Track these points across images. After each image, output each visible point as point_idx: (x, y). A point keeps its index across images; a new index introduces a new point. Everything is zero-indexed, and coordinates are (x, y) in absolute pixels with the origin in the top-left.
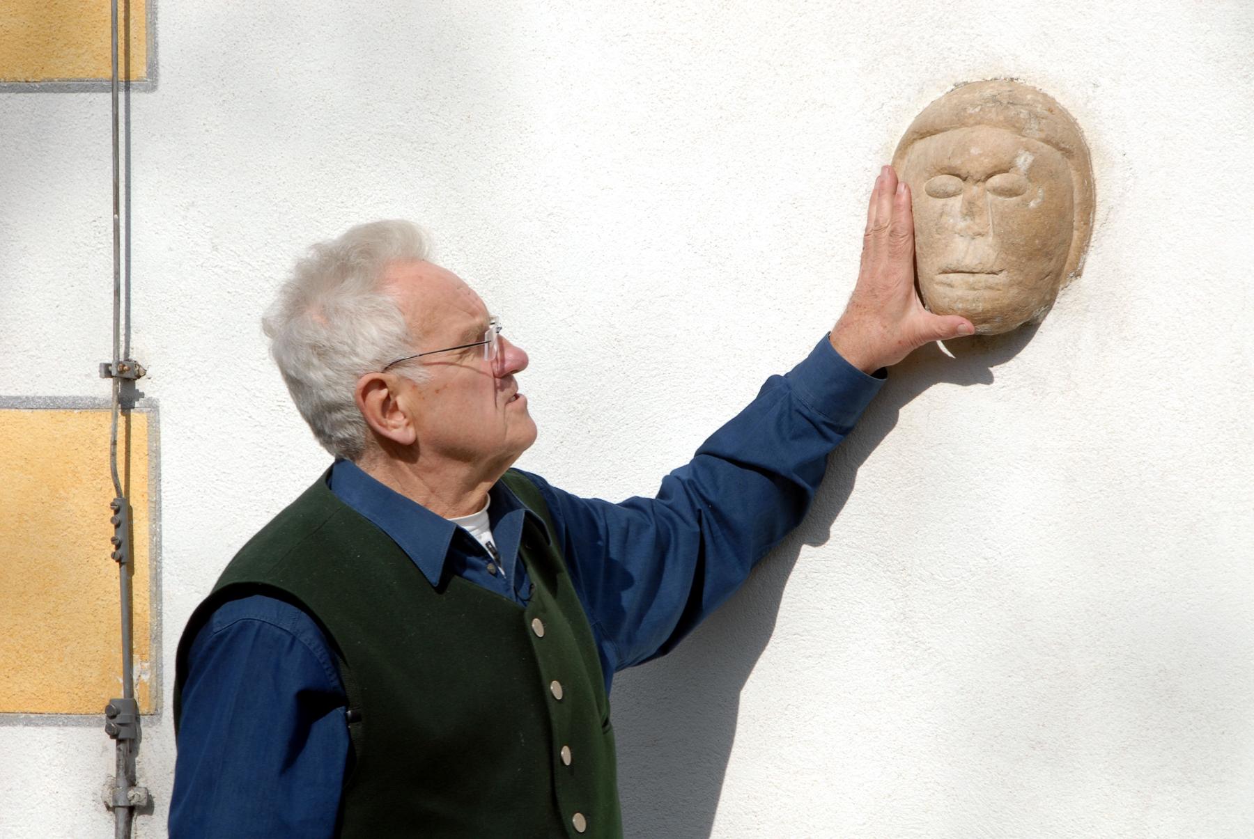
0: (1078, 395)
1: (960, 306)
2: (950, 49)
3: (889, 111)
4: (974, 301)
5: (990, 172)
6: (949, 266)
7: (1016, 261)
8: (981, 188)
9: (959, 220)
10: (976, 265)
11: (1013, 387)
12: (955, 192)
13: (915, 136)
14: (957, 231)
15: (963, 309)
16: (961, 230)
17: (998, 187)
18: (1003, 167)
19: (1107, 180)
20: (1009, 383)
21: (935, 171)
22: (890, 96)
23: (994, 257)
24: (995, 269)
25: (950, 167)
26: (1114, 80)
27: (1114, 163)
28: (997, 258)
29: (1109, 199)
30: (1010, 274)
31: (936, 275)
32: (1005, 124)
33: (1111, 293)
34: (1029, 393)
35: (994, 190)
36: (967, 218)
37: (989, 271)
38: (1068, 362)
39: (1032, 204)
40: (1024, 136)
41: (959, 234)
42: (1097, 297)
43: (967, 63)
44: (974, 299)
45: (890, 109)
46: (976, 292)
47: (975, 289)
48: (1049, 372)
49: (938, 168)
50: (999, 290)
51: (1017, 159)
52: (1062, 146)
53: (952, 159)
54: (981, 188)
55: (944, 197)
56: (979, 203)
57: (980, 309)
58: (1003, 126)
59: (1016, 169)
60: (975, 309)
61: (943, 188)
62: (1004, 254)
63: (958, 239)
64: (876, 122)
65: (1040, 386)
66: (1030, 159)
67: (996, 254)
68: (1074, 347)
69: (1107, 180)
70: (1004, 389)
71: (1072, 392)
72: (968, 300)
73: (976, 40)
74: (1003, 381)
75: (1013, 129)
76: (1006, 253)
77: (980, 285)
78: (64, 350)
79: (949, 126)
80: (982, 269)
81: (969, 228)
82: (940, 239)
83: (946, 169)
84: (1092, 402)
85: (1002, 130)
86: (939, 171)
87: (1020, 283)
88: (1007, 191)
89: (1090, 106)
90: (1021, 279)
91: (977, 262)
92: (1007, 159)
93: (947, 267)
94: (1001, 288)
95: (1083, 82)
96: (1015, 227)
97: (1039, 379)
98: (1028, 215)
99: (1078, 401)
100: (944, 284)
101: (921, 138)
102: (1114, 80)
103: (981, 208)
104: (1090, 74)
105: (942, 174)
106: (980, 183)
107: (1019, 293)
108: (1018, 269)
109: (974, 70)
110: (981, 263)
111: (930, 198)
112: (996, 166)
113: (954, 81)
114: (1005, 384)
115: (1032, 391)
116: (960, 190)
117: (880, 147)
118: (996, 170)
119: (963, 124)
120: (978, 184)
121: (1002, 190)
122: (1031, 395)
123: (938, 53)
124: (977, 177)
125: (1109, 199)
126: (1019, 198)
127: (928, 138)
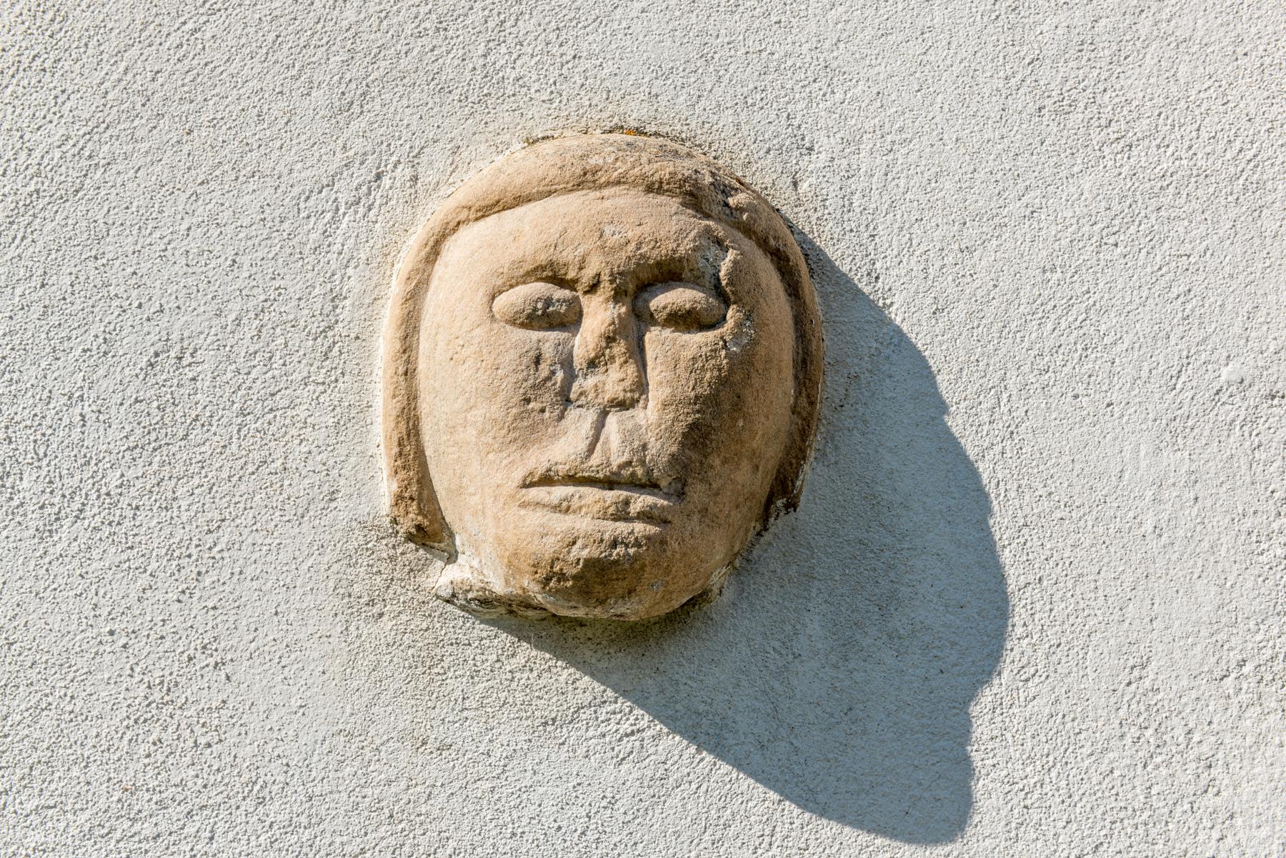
0: (797, 750)
13: (462, 216)
53: (560, 248)
86: (528, 274)
100: (544, 506)
101: (477, 219)
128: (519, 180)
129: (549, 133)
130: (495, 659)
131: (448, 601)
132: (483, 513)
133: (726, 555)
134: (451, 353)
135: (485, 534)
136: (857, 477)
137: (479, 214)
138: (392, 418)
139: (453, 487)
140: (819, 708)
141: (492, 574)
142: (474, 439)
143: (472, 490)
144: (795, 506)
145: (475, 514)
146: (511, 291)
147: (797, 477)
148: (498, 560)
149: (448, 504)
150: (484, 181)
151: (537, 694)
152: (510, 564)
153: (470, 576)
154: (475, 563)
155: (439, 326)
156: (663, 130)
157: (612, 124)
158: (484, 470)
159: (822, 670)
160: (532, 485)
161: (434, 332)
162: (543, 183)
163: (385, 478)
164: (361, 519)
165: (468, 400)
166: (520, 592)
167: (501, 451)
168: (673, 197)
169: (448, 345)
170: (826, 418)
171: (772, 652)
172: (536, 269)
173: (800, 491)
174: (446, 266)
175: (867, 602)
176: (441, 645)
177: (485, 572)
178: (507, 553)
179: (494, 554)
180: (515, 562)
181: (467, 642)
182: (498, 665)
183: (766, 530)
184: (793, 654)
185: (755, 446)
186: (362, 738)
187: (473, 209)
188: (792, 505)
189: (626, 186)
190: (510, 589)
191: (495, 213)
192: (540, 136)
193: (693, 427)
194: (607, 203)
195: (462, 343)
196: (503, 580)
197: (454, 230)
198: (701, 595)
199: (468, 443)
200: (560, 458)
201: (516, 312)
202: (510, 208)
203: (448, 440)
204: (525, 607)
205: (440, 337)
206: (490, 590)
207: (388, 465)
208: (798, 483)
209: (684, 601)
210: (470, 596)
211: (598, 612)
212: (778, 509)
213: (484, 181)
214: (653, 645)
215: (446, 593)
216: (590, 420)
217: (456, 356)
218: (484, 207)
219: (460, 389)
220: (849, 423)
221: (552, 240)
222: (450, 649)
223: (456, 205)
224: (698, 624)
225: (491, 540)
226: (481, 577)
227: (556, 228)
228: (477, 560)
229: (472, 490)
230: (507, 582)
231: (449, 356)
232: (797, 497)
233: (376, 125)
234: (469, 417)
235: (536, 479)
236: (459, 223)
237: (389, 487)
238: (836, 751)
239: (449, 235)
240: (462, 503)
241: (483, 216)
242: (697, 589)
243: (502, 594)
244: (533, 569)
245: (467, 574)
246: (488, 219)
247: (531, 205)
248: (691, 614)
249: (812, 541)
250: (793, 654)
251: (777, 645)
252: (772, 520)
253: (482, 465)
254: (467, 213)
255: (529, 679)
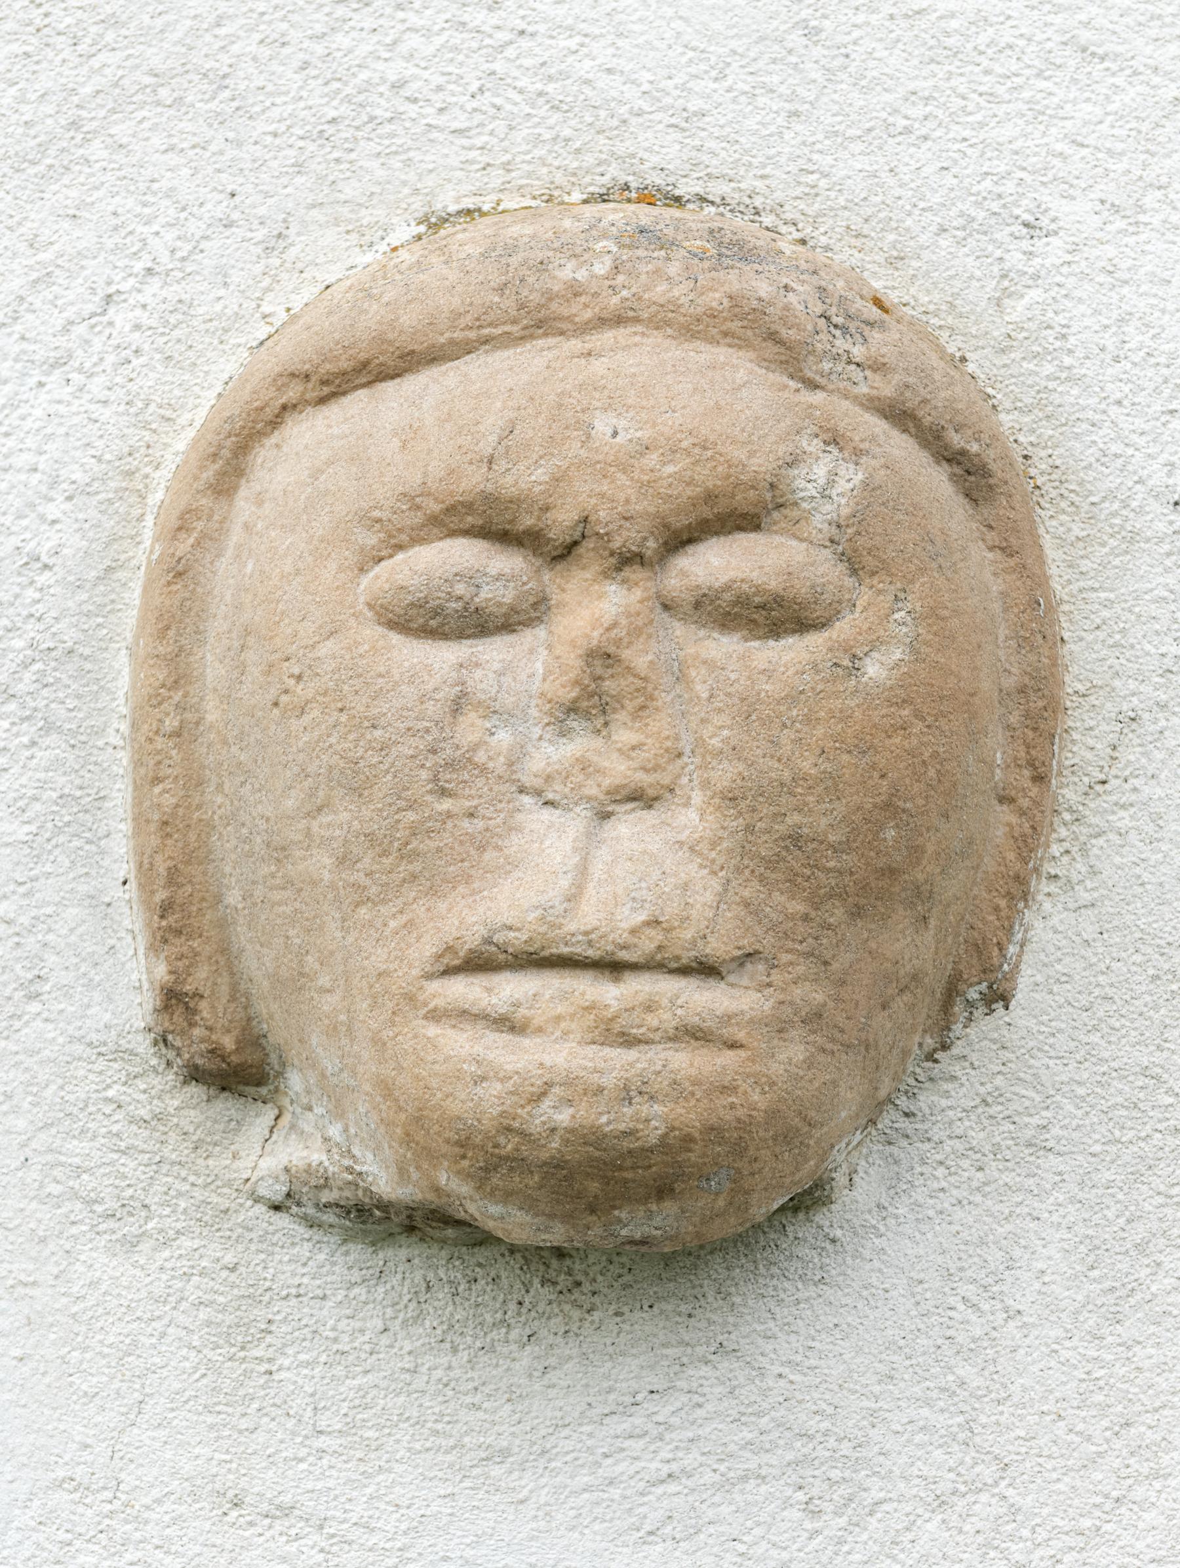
0: (1014, 1510)
1: (563, 1117)
2: (397, 86)
3: (137, 327)
4: (626, 1094)
5: (680, 522)
6: (498, 938)
7: (806, 918)
8: (638, 593)
9: (537, 731)
10: (633, 931)
11: (709, 1477)
12: (513, 609)
13: (292, 393)
14: (527, 780)
15: (571, 1131)
16: (549, 778)
17: (727, 588)
18: (743, 501)
19: (1107, 604)
20: (691, 1459)
21: (418, 518)
22: (139, 266)
23: (709, 897)
24: (717, 948)
25: (489, 499)
26: (1116, 209)
27: (1133, 537)
28: (721, 898)
29: (1117, 683)
30: (776, 977)
31: (429, 976)
32: (735, 326)
33: (1145, 1071)
34: (786, 1504)
35: (697, 605)
36: (573, 723)
37: (687, 957)
38: (965, 1371)
39: (874, 670)
40: (813, 386)
41: (538, 793)
42: (1081, 1091)
43: (479, 141)
44: (626, 1088)
45: (145, 319)
46: (632, 1054)
47: (629, 1041)
48: (873, 1413)
49: (436, 508)
50: (733, 1045)
51: (800, 471)
52: (956, 440)
53: (501, 465)
54: (638, 593)
55: (461, 635)
56: (639, 658)
57: (653, 1134)
58: (726, 334)
59: (794, 513)
60: (630, 1133)
61: (460, 589)
62: (755, 883)
63: (536, 818)
64: (80, 370)
65: (835, 1474)
66: (850, 478)
67: (716, 884)
68: (986, 1307)
69: (1107, 604)
70: (672, 1487)
71: (984, 1497)
72: (601, 1090)
73: (510, 52)
74: (665, 1454)
75: (771, 349)
76: (762, 879)
77: (652, 1020)
78: (233, 1270)
79: (472, 335)
80: (660, 948)
81: (584, 765)
82: (449, 815)
83: (469, 507)
84: (1080, 1541)
85: (722, 353)
86: (434, 520)
87: (814, 1018)
88: (762, 607)
89: (1017, 310)
90: (819, 997)
91: (642, 917)
92: (761, 464)
93: (488, 941)
94: (741, 1036)
95: (981, 215)
96: (806, 765)
97: (832, 1442)
98: (858, 714)
99: (1011, 1537)
100: (476, 1017)
101: (322, 401)
102: (1116, 209)
103: (645, 679)
104: (1009, 187)
105: (453, 534)
106: (634, 573)
107: (809, 1063)
108: (809, 954)
109: (507, 167)
110: (654, 923)
111: (395, 638)
112: (710, 497)
113: (418, 206)
114: (674, 1467)
115: (800, 1496)
116: (535, 606)
117: (97, 468)
118: (707, 513)
119: (539, 324)
120: (627, 572)
121: (742, 601)
122: (795, 1514)
123: (348, 99)
124: (627, 537)
125: (1117, 683)
126: (815, 641)
127: (362, 393)
128: (409, 319)
129: (468, 203)
130: (380, 1327)
131: (277, 1208)
132: (349, 1029)
133: (862, 1107)
134: (273, 692)
135: (354, 1074)
136: (1138, 935)
137: (326, 390)
138: (153, 827)
139: (284, 972)
140: (1061, 1424)
141: (370, 1156)
142: (327, 876)
143: (324, 981)
144: (1004, 998)
145: (332, 1031)
146: (400, 556)
147: (1009, 931)
148: (382, 1130)
149: (274, 1007)
150: (334, 319)
151: (468, 1400)
152: (408, 1139)
153: (324, 1158)
154: (335, 1131)
155: (247, 632)
156: (717, 190)
157: (605, 180)
158: (350, 939)
159: (1068, 1344)
160: (449, 972)
161: (236, 644)
162: (462, 322)
163: (141, 951)
164: (94, 1037)
165: (312, 793)
166: (431, 1196)
167: (384, 902)
168: (740, 347)
169: (268, 673)
170: (1070, 810)
171: (961, 1307)
172: (451, 510)
173: (1016, 967)
174: (260, 503)
175: (1160, 1200)
176: (266, 1298)
177: (356, 1151)
178: (403, 1116)
179: (374, 1116)
180: (420, 1136)
181: (319, 1292)
182: (385, 1340)
183: (945, 1047)
184: (1006, 1310)
185: (921, 877)
186: (108, 1495)
187: (314, 379)
188: (998, 997)
189: (639, 328)
190: (409, 1190)
191: (363, 386)
192: (452, 208)
193: (707, 521)
194: (598, 366)
195: (296, 671)
196: (393, 1169)
197: (275, 423)
198: (809, 1192)
199: (314, 883)
200: (508, 918)
201: (412, 605)
202: (392, 378)
203: (273, 876)
204: (439, 1220)
205: (250, 656)
206: (366, 1190)
207: (148, 925)
208: (1012, 950)
209: (776, 1206)
210: (326, 1197)
211: (595, 1233)
212: (970, 1004)
213: (334, 319)
214: (711, 1295)
215: (277, 1192)
216: (572, 833)
217: (284, 699)
218: (337, 375)
219: (296, 769)
220: (1123, 820)
221: (487, 445)
222: (285, 1307)
223: (277, 369)
224: (804, 1251)
225: (367, 1087)
226: (347, 1162)
227: (492, 423)
228: (339, 1126)
229: (324, 981)
230: (402, 1172)
231: (270, 696)
232: (1011, 977)
233: (100, 193)
234: (315, 828)
235: (457, 962)
236: (284, 407)
237: (149, 971)
238: (1098, 1513)
239: (262, 434)
240: (304, 1008)
241: (334, 395)
242: (803, 1179)
243: (393, 1197)
244: (457, 1150)
245: (317, 1156)
246: (346, 400)
247: (435, 371)
248: (789, 1229)
249: (1043, 1071)
250: (1006, 1310)
251: (969, 1290)
252: (957, 1028)
253: (346, 930)
254: (300, 388)
255: (449, 1368)
